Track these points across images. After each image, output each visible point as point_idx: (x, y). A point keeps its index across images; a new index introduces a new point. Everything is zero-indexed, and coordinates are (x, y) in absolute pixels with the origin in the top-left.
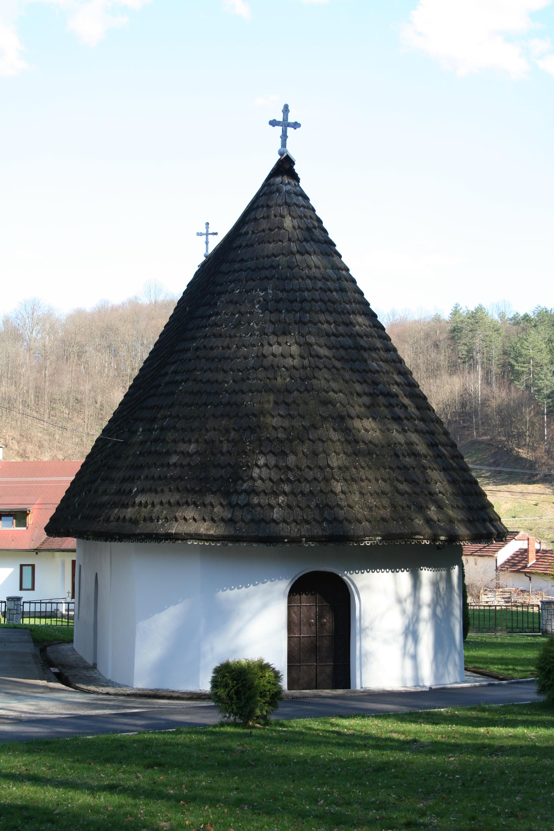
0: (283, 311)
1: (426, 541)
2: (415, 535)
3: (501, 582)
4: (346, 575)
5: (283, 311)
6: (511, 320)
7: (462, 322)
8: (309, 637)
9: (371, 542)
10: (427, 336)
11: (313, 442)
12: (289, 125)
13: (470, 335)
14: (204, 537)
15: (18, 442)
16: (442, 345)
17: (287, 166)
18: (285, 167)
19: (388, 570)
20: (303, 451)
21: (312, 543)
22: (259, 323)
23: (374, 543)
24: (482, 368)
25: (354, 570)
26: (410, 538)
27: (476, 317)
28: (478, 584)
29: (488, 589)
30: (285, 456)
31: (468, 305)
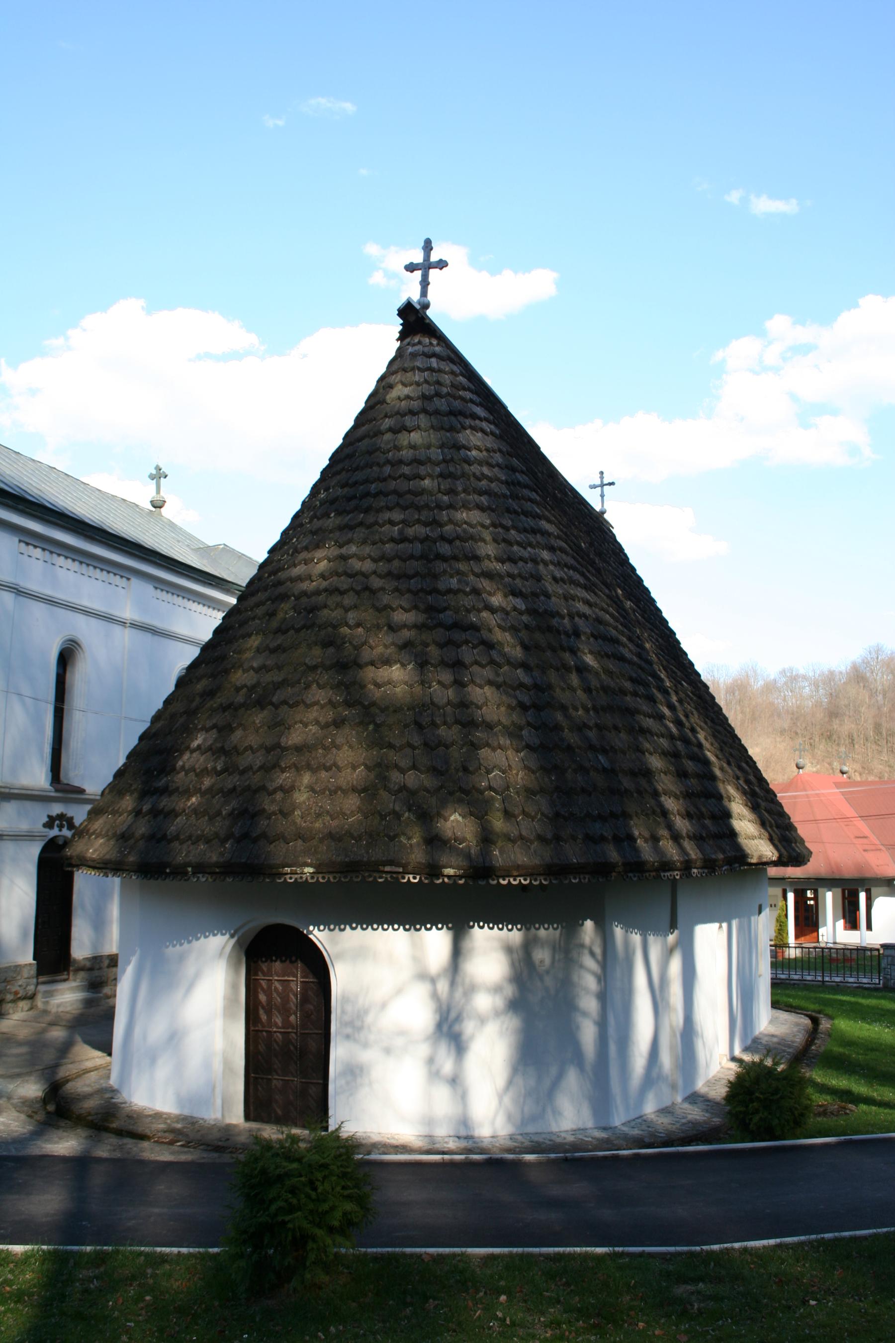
0: (332, 515)
1: (411, 876)
2: (384, 866)
5: (332, 515)
9: (296, 876)
11: (276, 707)
14: (90, 863)
15: (860, 774)
17: (412, 318)
18: (415, 320)
19: (396, 926)
25: (327, 924)
26: (374, 871)
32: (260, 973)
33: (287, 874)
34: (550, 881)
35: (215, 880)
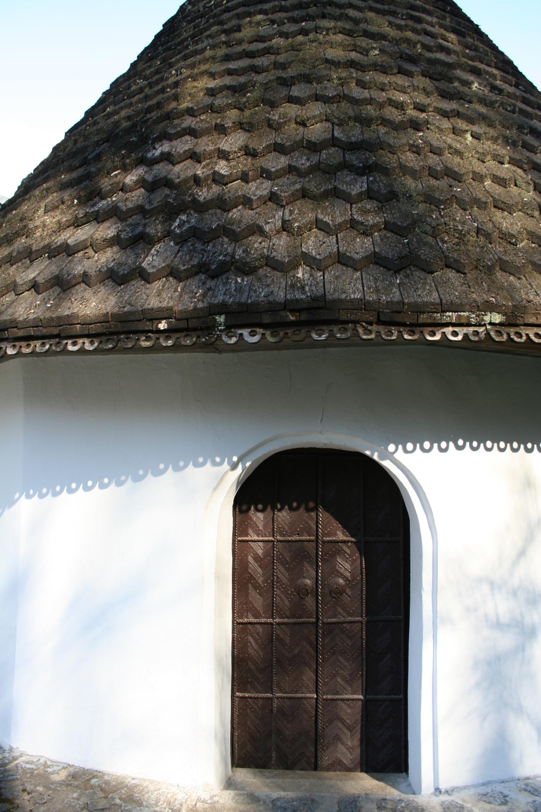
4: (390, 456)
8: (295, 624)
9: (465, 330)
23: (476, 333)
25: (418, 440)
32: (250, 531)
33: (447, 325)
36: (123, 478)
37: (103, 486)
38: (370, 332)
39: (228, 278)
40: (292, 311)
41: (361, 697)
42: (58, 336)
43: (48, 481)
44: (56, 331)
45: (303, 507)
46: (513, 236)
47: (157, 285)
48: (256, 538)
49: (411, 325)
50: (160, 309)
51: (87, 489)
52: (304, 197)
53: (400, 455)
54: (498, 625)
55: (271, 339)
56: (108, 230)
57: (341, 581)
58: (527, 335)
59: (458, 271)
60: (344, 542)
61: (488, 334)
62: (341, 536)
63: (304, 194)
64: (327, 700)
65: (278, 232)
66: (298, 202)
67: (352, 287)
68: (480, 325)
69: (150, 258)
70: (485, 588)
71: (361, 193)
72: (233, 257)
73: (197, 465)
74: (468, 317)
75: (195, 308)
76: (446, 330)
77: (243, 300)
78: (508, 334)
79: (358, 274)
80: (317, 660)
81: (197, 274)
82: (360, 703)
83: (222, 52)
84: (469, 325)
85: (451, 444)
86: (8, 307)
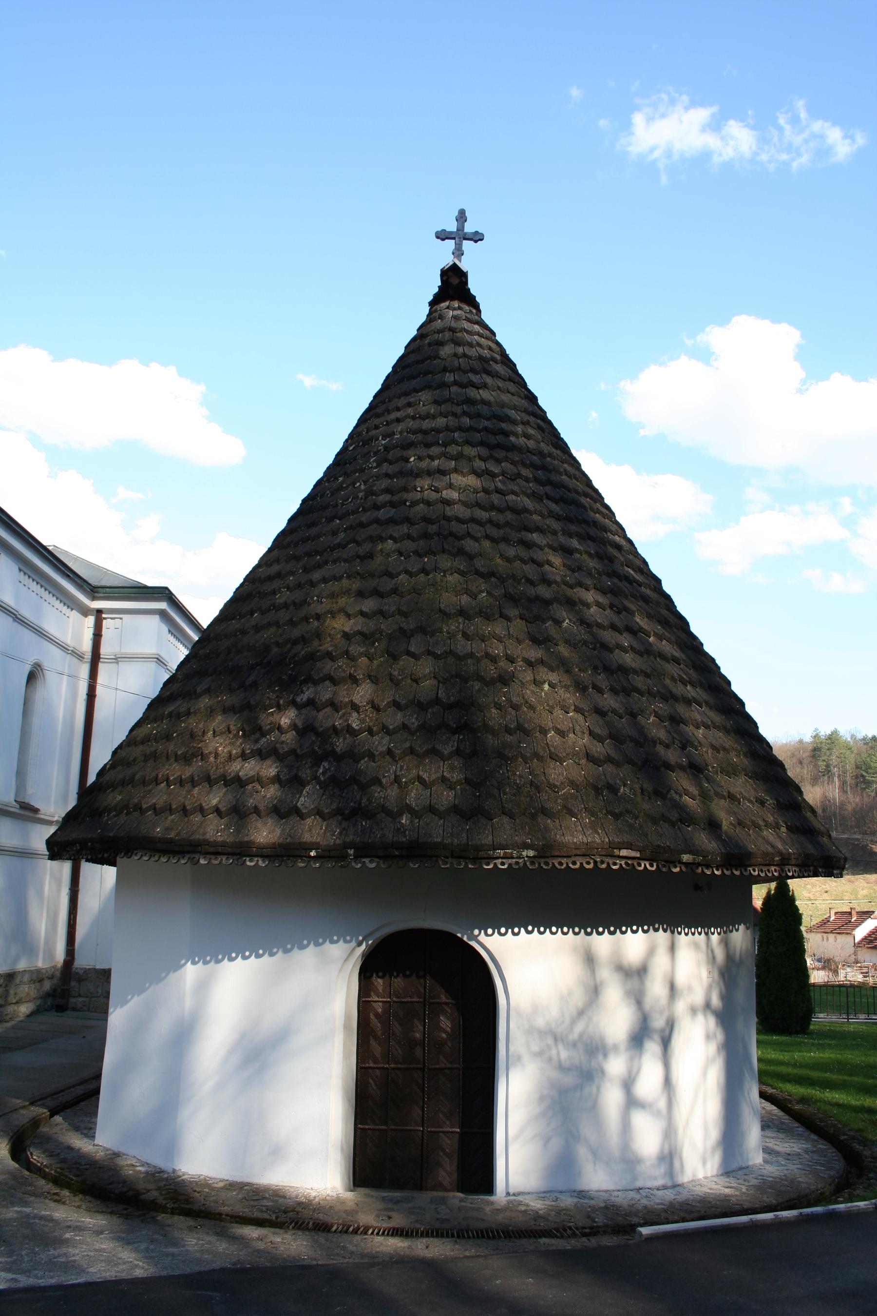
2: (620, 849)
3: (860, 957)
6: (861, 740)
7: (821, 743)
9: (510, 861)
10: (793, 755)
12: (461, 228)
13: (828, 753)
16: (805, 761)
17: (455, 281)
18: (454, 285)
20: (391, 674)
21: (371, 862)
22: (368, 481)
23: (517, 863)
24: (839, 780)
25: (496, 927)
27: (833, 738)
28: (837, 959)
29: (846, 964)
30: (354, 685)
31: (825, 731)
32: (372, 994)
33: (498, 858)
34: (723, 872)
35: (390, 867)
36: (275, 950)
37: (258, 956)
38: (447, 863)
39: (356, 821)
40: (396, 849)
41: (458, 1130)
42: (239, 854)
43: (215, 950)
44: (238, 851)
45: (414, 975)
46: (556, 786)
47: (309, 821)
48: (377, 999)
49: (473, 858)
50: (312, 843)
51: (245, 958)
52: (411, 753)
53: (482, 938)
54: (562, 1068)
55: (383, 866)
56: (270, 770)
57: (444, 1035)
58: (553, 863)
59: (510, 818)
60: (446, 1003)
61: (525, 864)
62: (443, 998)
63: (412, 751)
64: (431, 1132)
65: (392, 784)
66: (407, 758)
67: (438, 831)
68: (520, 858)
69: (302, 799)
70: (550, 1040)
71: (451, 753)
72: (360, 804)
73: (333, 942)
74: (512, 853)
75: (334, 844)
76: (496, 861)
77: (366, 841)
78: (539, 864)
79: (442, 822)
80: (424, 1099)
81: (335, 815)
82: (457, 1135)
83: (356, 585)
84: (512, 858)
85: (522, 930)
86: (199, 827)
